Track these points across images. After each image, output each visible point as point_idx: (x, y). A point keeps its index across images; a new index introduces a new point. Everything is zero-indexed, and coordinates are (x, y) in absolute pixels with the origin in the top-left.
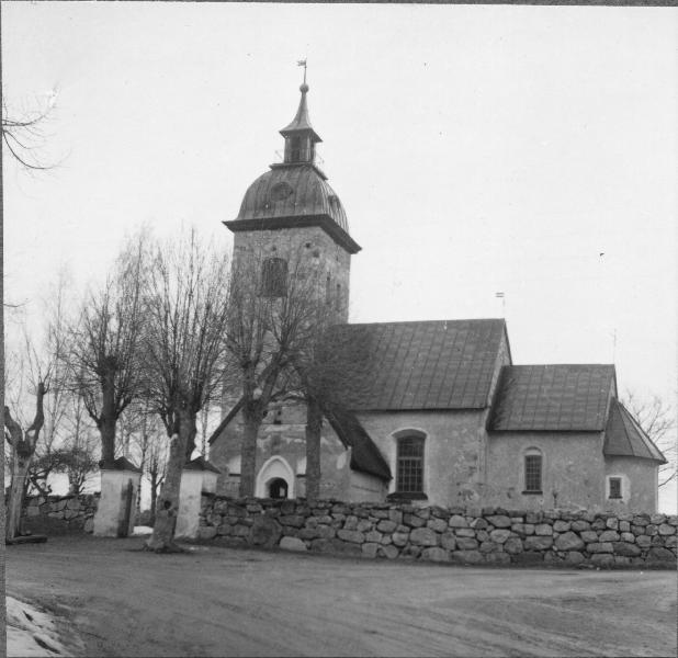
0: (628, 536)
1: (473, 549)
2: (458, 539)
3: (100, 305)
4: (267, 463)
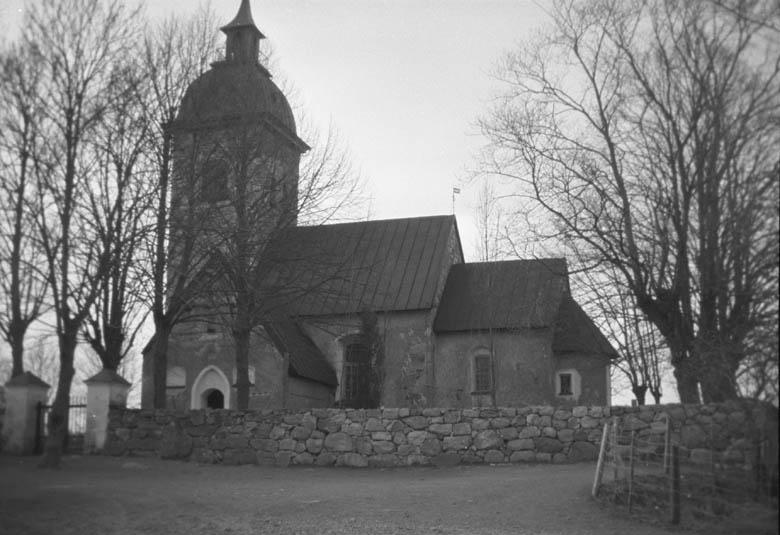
0: (550, 431)
1: (390, 453)
2: (374, 443)
3: (475, 244)
4: (204, 371)
